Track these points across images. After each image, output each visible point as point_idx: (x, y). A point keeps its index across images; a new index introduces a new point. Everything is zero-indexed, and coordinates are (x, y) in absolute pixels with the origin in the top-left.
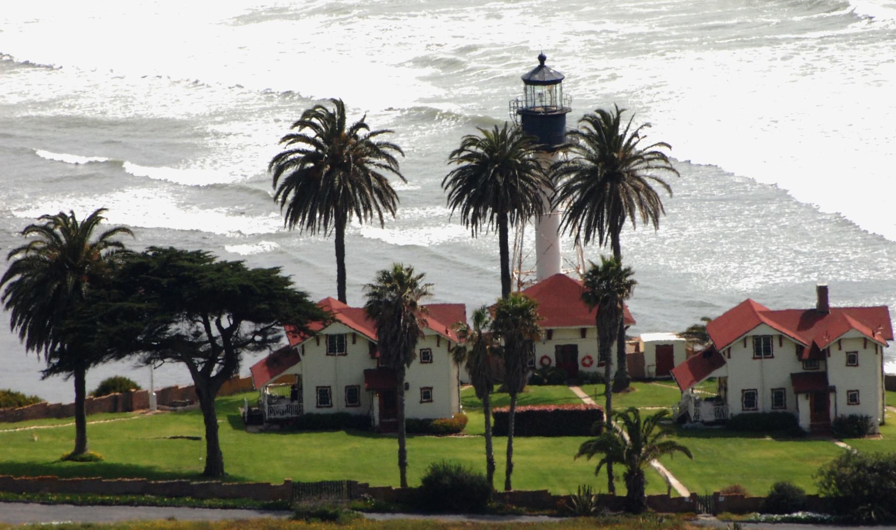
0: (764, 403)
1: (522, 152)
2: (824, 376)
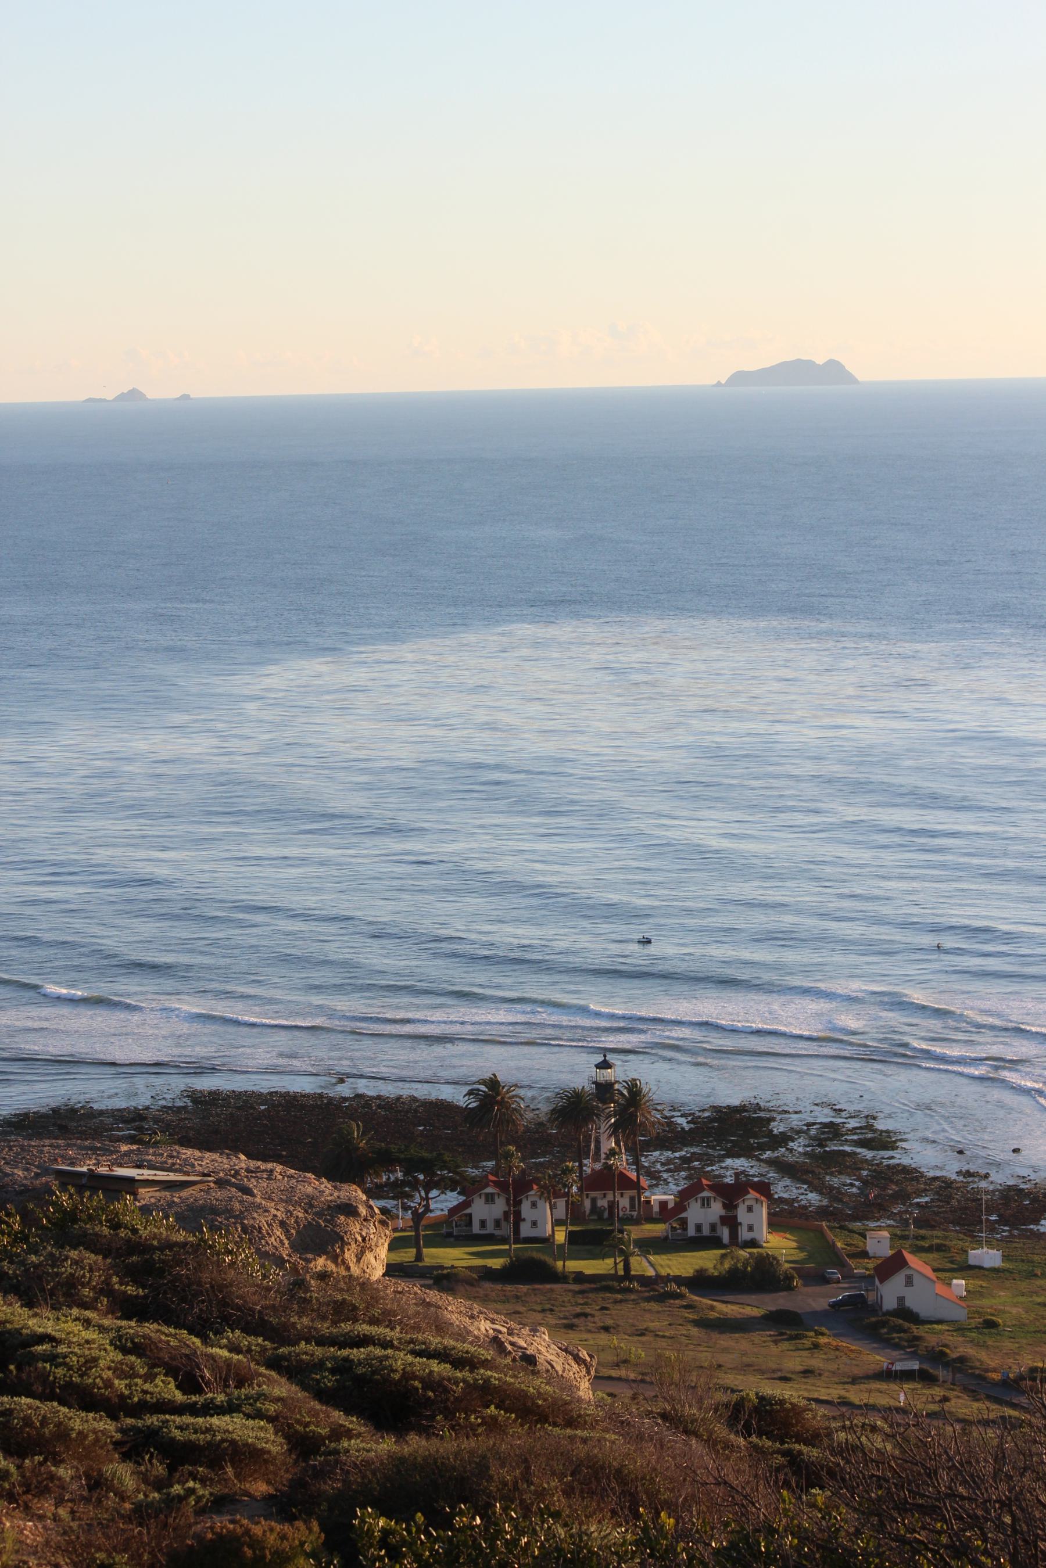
0: (706, 1231)
1: (49, 1220)
2: (736, 1217)
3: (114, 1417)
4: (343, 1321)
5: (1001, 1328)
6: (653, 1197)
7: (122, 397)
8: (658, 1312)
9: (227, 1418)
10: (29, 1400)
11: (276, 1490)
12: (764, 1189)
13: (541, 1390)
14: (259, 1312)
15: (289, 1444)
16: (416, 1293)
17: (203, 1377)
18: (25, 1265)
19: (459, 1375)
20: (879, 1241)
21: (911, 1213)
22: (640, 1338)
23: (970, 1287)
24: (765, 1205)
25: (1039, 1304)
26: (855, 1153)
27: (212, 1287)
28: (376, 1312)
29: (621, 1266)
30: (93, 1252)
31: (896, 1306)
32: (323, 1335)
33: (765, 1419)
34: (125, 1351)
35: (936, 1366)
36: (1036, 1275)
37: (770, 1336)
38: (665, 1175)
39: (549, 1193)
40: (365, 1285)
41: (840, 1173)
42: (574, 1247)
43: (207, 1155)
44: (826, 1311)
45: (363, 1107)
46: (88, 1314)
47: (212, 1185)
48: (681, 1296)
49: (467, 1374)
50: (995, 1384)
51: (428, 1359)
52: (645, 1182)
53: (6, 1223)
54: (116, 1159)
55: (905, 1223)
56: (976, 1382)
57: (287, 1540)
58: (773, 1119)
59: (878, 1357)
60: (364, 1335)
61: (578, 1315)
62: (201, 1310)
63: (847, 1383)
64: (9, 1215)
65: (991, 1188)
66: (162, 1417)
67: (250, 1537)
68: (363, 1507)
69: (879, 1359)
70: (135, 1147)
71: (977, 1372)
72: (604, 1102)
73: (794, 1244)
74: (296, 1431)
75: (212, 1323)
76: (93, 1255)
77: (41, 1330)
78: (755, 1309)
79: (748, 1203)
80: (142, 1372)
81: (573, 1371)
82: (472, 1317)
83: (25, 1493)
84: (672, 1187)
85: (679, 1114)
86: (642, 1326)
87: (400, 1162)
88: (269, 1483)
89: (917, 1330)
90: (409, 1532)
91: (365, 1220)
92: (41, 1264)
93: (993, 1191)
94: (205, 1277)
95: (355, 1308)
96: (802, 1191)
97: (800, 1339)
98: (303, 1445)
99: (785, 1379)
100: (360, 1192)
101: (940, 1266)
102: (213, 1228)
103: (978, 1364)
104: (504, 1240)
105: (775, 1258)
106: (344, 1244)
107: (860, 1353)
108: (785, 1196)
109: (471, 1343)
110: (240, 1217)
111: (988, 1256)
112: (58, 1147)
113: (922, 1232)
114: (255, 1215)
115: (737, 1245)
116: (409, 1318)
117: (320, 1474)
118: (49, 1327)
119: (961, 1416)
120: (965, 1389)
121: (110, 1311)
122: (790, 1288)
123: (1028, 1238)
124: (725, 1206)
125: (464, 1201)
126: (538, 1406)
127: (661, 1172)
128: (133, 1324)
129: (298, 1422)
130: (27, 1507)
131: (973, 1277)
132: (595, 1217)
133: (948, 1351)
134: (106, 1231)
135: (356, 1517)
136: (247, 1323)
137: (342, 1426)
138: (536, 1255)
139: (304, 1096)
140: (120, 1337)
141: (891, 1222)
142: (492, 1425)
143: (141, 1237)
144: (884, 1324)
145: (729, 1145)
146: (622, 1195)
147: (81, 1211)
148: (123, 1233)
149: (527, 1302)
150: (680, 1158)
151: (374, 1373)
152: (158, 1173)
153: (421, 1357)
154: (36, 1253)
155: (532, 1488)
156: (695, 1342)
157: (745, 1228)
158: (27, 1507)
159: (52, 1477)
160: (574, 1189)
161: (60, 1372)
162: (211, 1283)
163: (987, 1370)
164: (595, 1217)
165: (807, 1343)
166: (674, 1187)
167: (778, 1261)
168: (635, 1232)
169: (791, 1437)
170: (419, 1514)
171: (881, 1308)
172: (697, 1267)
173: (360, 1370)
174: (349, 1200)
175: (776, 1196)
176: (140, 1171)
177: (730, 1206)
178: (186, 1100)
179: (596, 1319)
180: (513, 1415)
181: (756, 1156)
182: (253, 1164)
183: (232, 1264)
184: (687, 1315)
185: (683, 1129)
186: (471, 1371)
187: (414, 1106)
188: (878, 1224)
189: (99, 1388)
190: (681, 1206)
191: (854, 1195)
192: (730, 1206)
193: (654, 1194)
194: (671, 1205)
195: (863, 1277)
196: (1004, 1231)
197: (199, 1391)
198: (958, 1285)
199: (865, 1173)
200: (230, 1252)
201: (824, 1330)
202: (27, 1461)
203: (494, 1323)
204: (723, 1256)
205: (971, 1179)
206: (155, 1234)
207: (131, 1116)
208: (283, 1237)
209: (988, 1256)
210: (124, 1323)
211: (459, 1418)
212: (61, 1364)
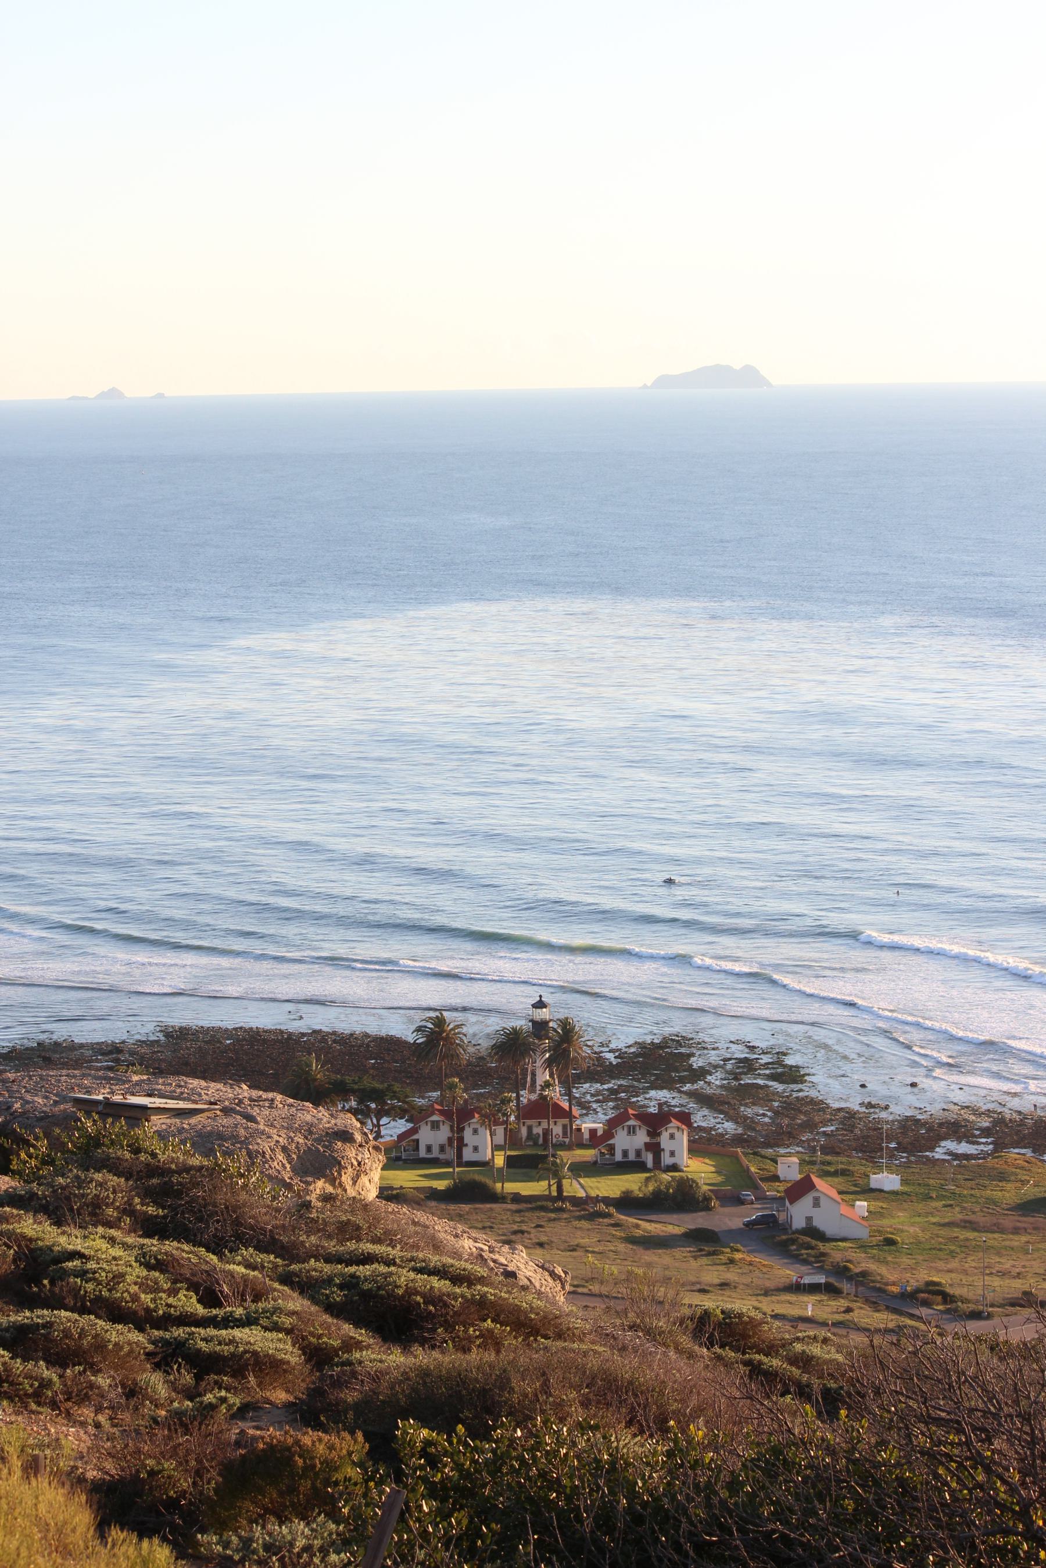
0: (632, 1157)
1: (74, 1146)
2: (659, 1144)
3: (141, 1330)
5: (900, 1245)
6: (584, 1125)
7: (103, 395)
8: (588, 1230)
9: (247, 1330)
10: (68, 1314)
11: (296, 1398)
12: (685, 1118)
14: (271, 1231)
15: (304, 1354)
16: (405, 1214)
17: (222, 1292)
18: (53, 1187)
19: (458, 1290)
20: (789, 1166)
21: (818, 1141)
23: (872, 1209)
24: (685, 1133)
25: (934, 1224)
26: (767, 1086)
27: (227, 1208)
28: (379, 1232)
29: (554, 1188)
30: (115, 1175)
31: (804, 1225)
32: (330, 1253)
33: (725, 1333)
34: (149, 1267)
35: (838, 1281)
36: (931, 1198)
37: (690, 1252)
38: (594, 1106)
40: (366, 1207)
41: (754, 1104)
42: (511, 1170)
43: (212, 1085)
44: (740, 1229)
45: (320, 1042)
46: (113, 1232)
47: (218, 1112)
48: (609, 1215)
50: (895, 1296)
52: (576, 1111)
53: (34, 1146)
54: (129, 1088)
55: (813, 1150)
56: (877, 1295)
57: (335, 1449)
58: (692, 1055)
59: (788, 1272)
61: (515, 1233)
62: (216, 1229)
64: (37, 1139)
65: (891, 1118)
66: (187, 1329)
67: (300, 1446)
68: (405, 1419)
69: (788, 1272)
70: (145, 1077)
71: (878, 1285)
72: (540, 1038)
74: (310, 1343)
75: (227, 1241)
76: (115, 1178)
77: (71, 1247)
79: (472, 1126)
80: (166, 1286)
82: (456, 1236)
83: (68, 1400)
84: (601, 1116)
86: (574, 1242)
87: (353, 1092)
88: (288, 1391)
89: (822, 1247)
90: (451, 1443)
92: (67, 1186)
93: (893, 1121)
94: (220, 1198)
95: (358, 1228)
96: (719, 1120)
98: (318, 1356)
100: (354, 1120)
101: (844, 1189)
102: (225, 1154)
103: (879, 1278)
104: (448, 1164)
105: (693, 1181)
106: (341, 1168)
107: (771, 1267)
108: (704, 1124)
109: (466, 1261)
110: (245, 1142)
111: (887, 1180)
112: (74, 1077)
113: (829, 1158)
114: (259, 1141)
117: (338, 1383)
118: (77, 1244)
119: (864, 1325)
120: (867, 1301)
121: (132, 1230)
122: (708, 1208)
123: (924, 1164)
124: (649, 1134)
126: (532, 1320)
127: (590, 1102)
128: (155, 1242)
129: (312, 1334)
130: (68, 1414)
131: (874, 1199)
133: (851, 1266)
134: (128, 1155)
135: (398, 1428)
136: (259, 1241)
137: (352, 1338)
139: (266, 1031)
140: (144, 1255)
141: (800, 1149)
142: (491, 1341)
143: (159, 1161)
144: (793, 1241)
145: (653, 1078)
146: (555, 1123)
147: (104, 1136)
148: (143, 1157)
151: (379, 1288)
152: (169, 1101)
154: (63, 1175)
155: (551, 1399)
157: (667, 1154)
158: (68, 1414)
159: (92, 1386)
160: (512, 1118)
161: (90, 1286)
162: (225, 1204)
163: (887, 1284)
164: (531, 1143)
166: (602, 1116)
167: (697, 1184)
168: (568, 1157)
169: (750, 1348)
170: (460, 1426)
171: (791, 1226)
172: (623, 1189)
173: (366, 1286)
175: (695, 1125)
176: (152, 1100)
177: (654, 1133)
178: (158, 1034)
180: (508, 1328)
182: (255, 1093)
183: (245, 1186)
185: (611, 1063)
186: (469, 1287)
188: (788, 1150)
189: (127, 1302)
190: (609, 1134)
191: (766, 1124)
192: (654, 1133)
194: (600, 1133)
195: (774, 1199)
196: (903, 1157)
197: (219, 1305)
198: (861, 1207)
199: (776, 1104)
200: (242, 1176)
202: (68, 1371)
204: (648, 1179)
205: (872, 1110)
206: (173, 1158)
207: (109, 1048)
208: (285, 1162)
209: (887, 1180)
210: (146, 1241)
212: (90, 1280)
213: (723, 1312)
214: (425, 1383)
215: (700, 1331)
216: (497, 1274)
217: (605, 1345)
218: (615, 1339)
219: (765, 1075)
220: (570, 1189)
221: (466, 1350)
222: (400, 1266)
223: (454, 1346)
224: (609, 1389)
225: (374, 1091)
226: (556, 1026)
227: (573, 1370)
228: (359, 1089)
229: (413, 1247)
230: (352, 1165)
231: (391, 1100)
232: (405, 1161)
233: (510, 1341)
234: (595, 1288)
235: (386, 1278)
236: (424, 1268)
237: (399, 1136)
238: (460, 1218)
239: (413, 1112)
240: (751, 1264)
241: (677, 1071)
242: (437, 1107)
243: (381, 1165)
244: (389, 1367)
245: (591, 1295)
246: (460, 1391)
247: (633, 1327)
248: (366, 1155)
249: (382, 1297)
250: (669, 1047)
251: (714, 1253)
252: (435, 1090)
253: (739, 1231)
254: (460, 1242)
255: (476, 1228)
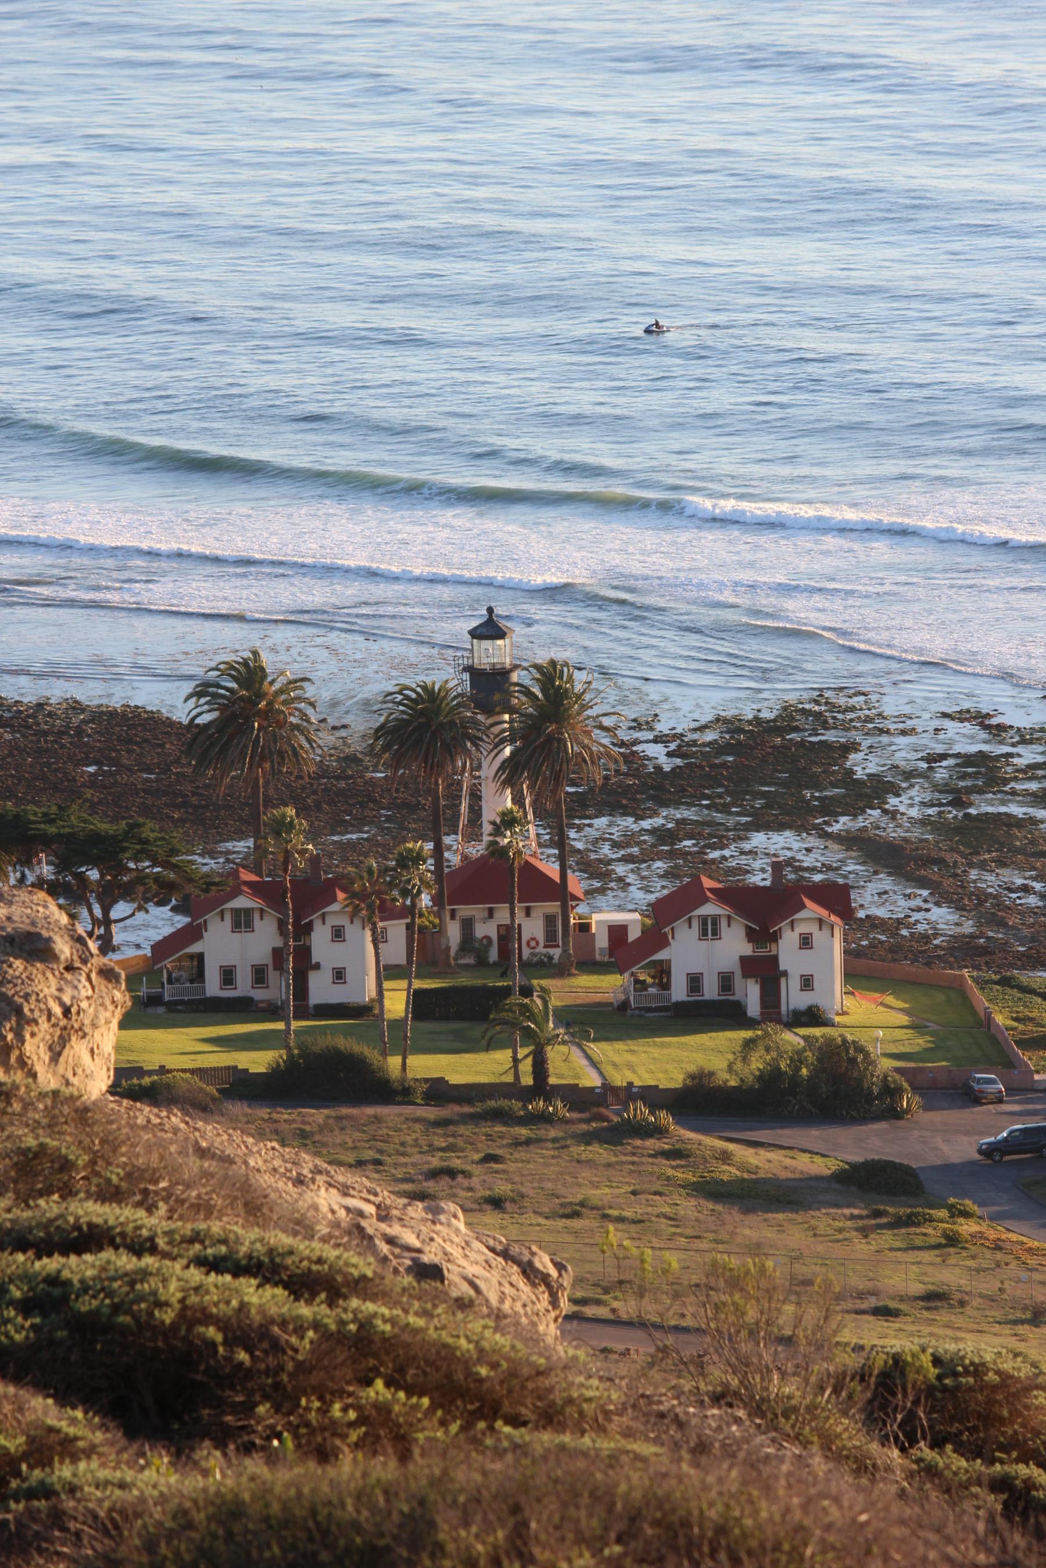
0: (711, 991)
2: (775, 959)
4: (41, 1194)
6: (596, 917)
8: (609, 1165)
12: (836, 898)
13: (485, 1345)
16: (176, 1131)
22: (568, 1222)
29: (526, 1066)
37: (852, 1217)
38: (620, 869)
39: (370, 907)
40: (83, 1114)
41: (1002, 863)
44: (972, 1163)
48: (658, 1131)
49: (324, 1309)
51: (235, 1275)
52: (577, 884)
58: (852, 747)
60: (90, 1225)
61: (434, 1174)
63: (1023, 1322)
72: (489, 711)
73: (904, 1020)
78: (818, 1159)
79: (331, 921)
81: (518, 1297)
82: (299, 1181)
85: (650, 736)
87: (46, 842)
91: (69, 968)
95: (66, 1165)
96: (918, 902)
97: (918, 1225)
99: (884, 1312)
104: (273, 1012)
105: (860, 1049)
106: (22, 1021)
108: (881, 912)
109: (324, 1240)
115: (779, 1021)
116: (188, 1186)
122: (894, 1114)
124: (751, 936)
125: (187, 928)
126: (480, 1381)
127: (609, 862)
132: (470, 960)
137: (51, 1430)
138: (342, 1043)
142: (383, 1431)
145: (758, 803)
146: (528, 912)
149: (325, 1145)
150: (653, 832)
151: (116, 1309)
153: (219, 1271)
156: (689, 1232)
157: (795, 983)
160: (425, 900)
164: (470, 960)
165: (932, 1233)
167: (867, 1055)
169: (1002, 1448)
172: (692, 1068)
173: (86, 1305)
174: (33, 923)
175: (861, 914)
177: (763, 934)
179: (475, 1181)
180: (426, 1401)
181: (816, 827)
184: (670, 1172)
185: (658, 768)
186: (331, 1304)
187: (75, 721)
190: (655, 937)
191: (1032, 911)
192: (763, 934)
193: (600, 910)
194: (634, 934)
201: (974, 1208)
203: (346, 1195)
211: (308, 1409)
213: (937, 1361)
214: (230, 1535)
215: (883, 1407)
216: (396, 1271)
217: (656, 1441)
218: (681, 1425)
219: (1027, 793)
220: (563, 1068)
221: (325, 1455)
222: (166, 1255)
223: (298, 1446)
224: (675, 1548)
225: (96, 838)
226: (527, 682)
227: (585, 1500)
228: (59, 836)
229: (196, 1207)
230: (50, 1015)
231: (136, 860)
232: (173, 1006)
233: (430, 1433)
234: (626, 1307)
235: (132, 1284)
236: (224, 1258)
237: (157, 947)
238: (303, 1138)
239: (190, 889)
240: (998, 1246)
241: (817, 786)
242: (247, 876)
243: (119, 1013)
244: (142, 1499)
245: (616, 1322)
246: (315, 1554)
247: (721, 1397)
248: (82, 989)
249: (123, 1329)
250: (796, 729)
251: (909, 1221)
252: (241, 836)
253: (969, 1169)
254: (309, 1196)
255: (340, 1164)
